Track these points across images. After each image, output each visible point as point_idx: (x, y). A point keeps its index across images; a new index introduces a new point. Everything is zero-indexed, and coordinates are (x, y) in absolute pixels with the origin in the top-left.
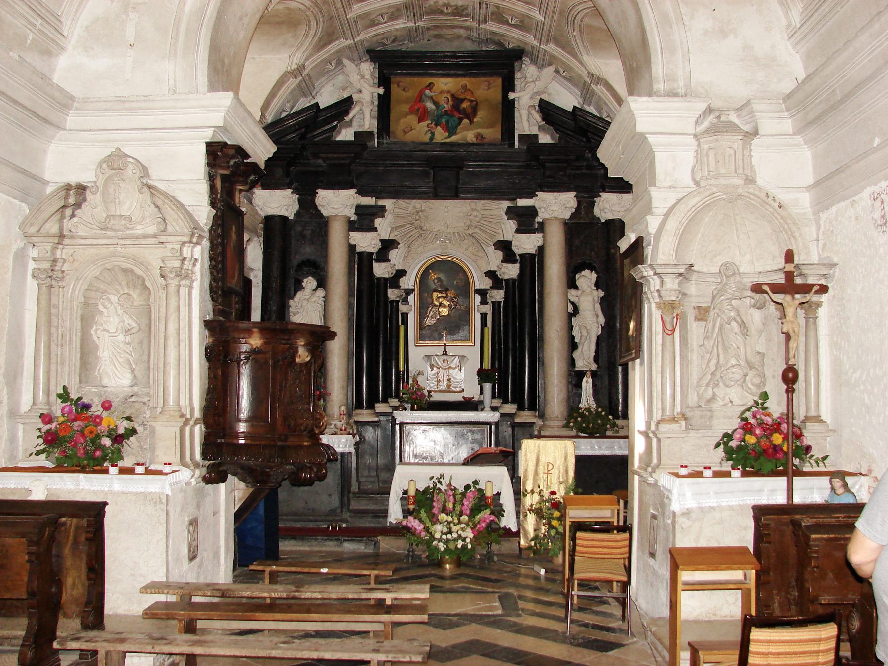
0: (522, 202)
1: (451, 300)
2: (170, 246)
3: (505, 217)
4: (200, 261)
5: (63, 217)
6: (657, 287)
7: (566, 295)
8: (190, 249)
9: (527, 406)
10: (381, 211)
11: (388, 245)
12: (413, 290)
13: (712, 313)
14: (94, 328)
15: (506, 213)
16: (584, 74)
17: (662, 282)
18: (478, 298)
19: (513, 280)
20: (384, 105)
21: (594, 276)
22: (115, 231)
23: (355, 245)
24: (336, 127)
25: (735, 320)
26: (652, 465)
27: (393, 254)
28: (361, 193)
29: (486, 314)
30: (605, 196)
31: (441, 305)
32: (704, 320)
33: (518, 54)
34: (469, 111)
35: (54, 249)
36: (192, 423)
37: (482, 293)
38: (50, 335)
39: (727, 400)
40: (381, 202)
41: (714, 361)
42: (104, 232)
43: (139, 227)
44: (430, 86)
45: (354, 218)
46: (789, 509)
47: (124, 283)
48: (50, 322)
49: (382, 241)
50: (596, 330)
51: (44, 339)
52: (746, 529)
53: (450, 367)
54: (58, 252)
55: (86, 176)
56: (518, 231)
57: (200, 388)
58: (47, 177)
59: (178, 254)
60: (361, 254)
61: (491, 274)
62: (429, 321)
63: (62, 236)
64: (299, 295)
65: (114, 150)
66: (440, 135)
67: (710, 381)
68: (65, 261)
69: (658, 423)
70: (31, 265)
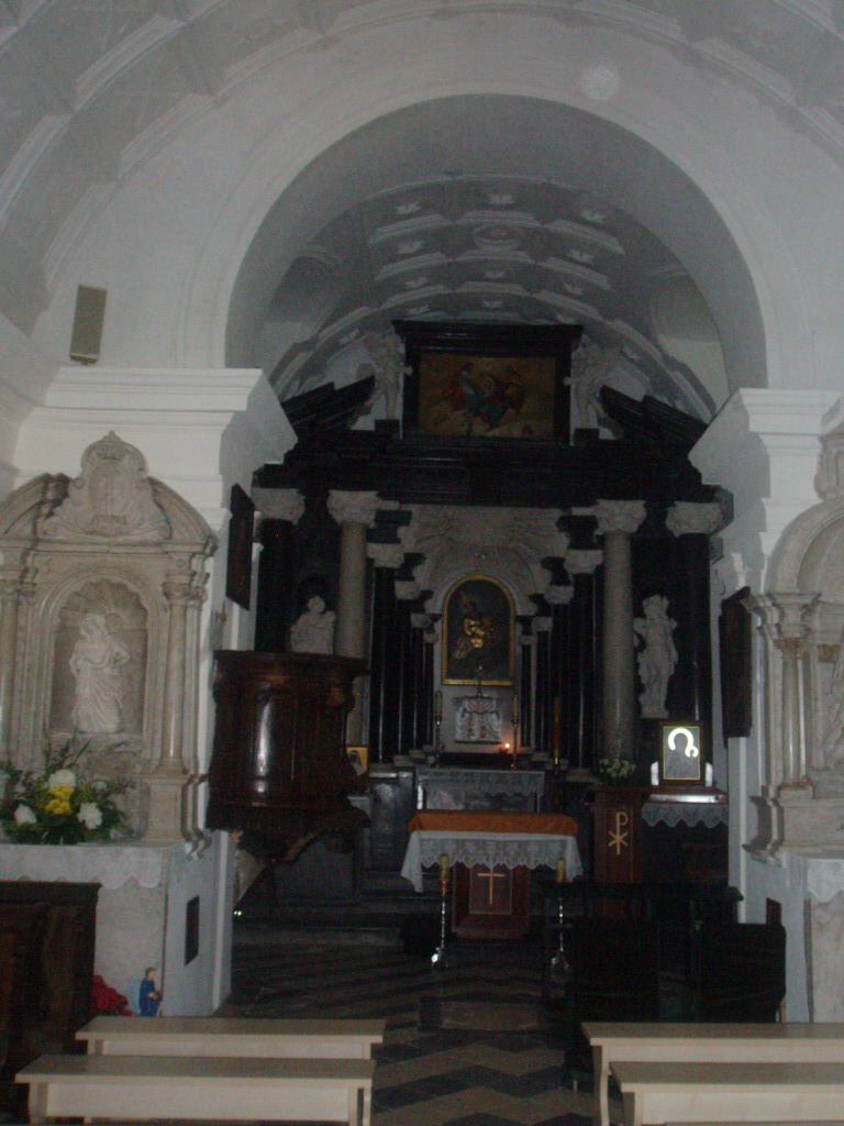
0: (578, 511)
2: (176, 557)
3: (555, 528)
5: (38, 516)
10: (405, 518)
11: (412, 560)
12: (441, 615)
15: (558, 524)
16: (657, 355)
17: (782, 616)
18: (519, 627)
19: (565, 606)
20: (412, 392)
21: (666, 602)
24: (352, 413)
27: (421, 574)
28: (383, 495)
31: (474, 635)
35: (25, 554)
36: (197, 780)
37: (525, 621)
40: (405, 508)
44: (468, 367)
45: (373, 525)
53: (486, 712)
54: (29, 559)
55: (73, 469)
60: (379, 570)
61: (537, 599)
62: (458, 655)
63: (36, 541)
64: (303, 619)
65: (106, 434)
66: (480, 429)
68: (37, 571)
69: (780, 788)
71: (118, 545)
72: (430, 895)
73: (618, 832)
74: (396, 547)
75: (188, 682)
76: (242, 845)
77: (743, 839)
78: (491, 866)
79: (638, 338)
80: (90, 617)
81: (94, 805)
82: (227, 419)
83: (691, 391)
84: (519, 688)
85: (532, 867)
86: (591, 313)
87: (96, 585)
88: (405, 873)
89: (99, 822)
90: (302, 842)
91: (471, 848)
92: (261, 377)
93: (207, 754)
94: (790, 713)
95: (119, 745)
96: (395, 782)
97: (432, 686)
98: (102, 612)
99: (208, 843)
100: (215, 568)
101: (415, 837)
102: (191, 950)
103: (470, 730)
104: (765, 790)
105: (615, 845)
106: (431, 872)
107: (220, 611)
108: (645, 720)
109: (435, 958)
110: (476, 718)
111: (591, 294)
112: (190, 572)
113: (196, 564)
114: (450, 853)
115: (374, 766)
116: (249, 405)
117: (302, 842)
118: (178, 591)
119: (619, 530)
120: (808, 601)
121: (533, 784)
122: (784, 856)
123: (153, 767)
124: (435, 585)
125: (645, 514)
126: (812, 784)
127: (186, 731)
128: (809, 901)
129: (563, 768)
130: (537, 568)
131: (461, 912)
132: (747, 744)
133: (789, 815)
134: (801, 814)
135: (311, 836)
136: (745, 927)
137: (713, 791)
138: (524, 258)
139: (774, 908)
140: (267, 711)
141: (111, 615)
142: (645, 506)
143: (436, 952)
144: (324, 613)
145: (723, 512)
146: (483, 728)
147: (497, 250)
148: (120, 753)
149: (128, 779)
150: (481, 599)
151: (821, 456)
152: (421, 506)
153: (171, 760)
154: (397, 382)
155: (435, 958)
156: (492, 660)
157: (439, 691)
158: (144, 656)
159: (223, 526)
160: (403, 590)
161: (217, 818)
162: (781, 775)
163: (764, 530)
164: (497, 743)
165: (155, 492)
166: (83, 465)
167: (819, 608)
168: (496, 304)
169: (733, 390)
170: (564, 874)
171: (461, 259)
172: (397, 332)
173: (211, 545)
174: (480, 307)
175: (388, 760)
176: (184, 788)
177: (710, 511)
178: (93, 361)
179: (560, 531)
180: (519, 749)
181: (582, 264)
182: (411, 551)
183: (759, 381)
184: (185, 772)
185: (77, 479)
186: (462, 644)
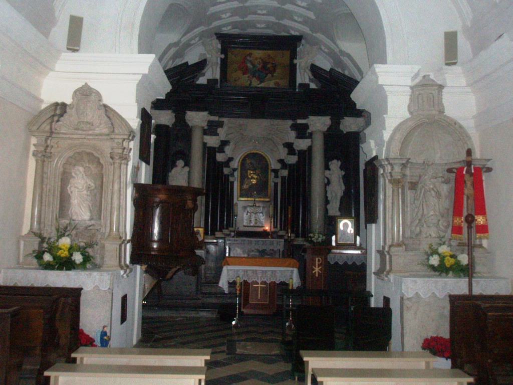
0: (299, 121)
1: (258, 175)
2: (116, 141)
3: (290, 129)
5: (51, 123)
6: (390, 171)
8: (127, 143)
10: (221, 124)
11: (224, 143)
13: (420, 186)
14: (69, 186)
15: (290, 127)
16: (337, 50)
17: (392, 169)
19: (294, 165)
20: (224, 64)
21: (339, 163)
22: (83, 130)
23: (206, 143)
24: (197, 76)
25: (433, 189)
26: (386, 270)
27: (228, 149)
28: (211, 114)
29: (277, 183)
30: (346, 118)
31: (252, 178)
32: (415, 190)
33: (298, 39)
34: (271, 69)
35: (46, 140)
36: (126, 242)
37: (276, 171)
38: (42, 189)
39: (428, 235)
41: (421, 213)
43: (97, 129)
44: (250, 55)
48: (42, 182)
49: (222, 141)
50: (340, 194)
51: (38, 191)
52: (444, 308)
54: (49, 142)
55: (68, 100)
57: (130, 225)
58: (42, 97)
59: (121, 145)
60: (210, 148)
61: (281, 161)
62: (245, 187)
63: (52, 133)
65: (84, 84)
66: (255, 83)
67: (418, 224)
68: (52, 147)
69: (390, 246)
70: (32, 148)
72: (232, 294)
73: (317, 267)
74: (217, 137)
75: (122, 197)
76: (146, 271)
78: (259, 281)
80: (77, 168)
81: (79, 253)
82: (139, 77)
86: (305, 29)
87: (79, 153)
88: (220, 284)
89: (81, 260)
90: (174, 270)
95: (90, 226)
96: (216, 244)
100: (134, 146)
101: (225, 269)
102: (124, 318)
103: (250, 221)
104: (384, 247)
105: (315, 273)
106: (232, 284)
107: (136, 166)
109: (234, 323)
110: (253, 215)
111: (306, 21)
117: (174, 270)
120: (404, 162)
121: (279, 245)
122: (391, 277)
124: (235, 154)
129: (292, 238)
130: (281, 147)
132: (376, 227)
134: (400, 258)
135: (178, 267)
139: (387, 300)
140: (158, 211)
143: (234, 320)
145: (366, 122)
146: (256, 220)
148: (90, 229)
149: (95, 241)
150: (256, 161)
151: (411, 96)
155: (234, 323)
156: (261, 189)
157: (236, 203)
159: (138, 126)
160: (220, 157)
161: (135, 259)
163: (385, 130)
164: (263, 227)
165: (106, 111)
166: (73, 98)
168: (263, 26)
169: (371, 65)
176: (120, 246)
177: (360, 121)
178: (77, 50)
179: (292, 130)
180: (273, 230)
183: (384, 61)
184: (121, 238)
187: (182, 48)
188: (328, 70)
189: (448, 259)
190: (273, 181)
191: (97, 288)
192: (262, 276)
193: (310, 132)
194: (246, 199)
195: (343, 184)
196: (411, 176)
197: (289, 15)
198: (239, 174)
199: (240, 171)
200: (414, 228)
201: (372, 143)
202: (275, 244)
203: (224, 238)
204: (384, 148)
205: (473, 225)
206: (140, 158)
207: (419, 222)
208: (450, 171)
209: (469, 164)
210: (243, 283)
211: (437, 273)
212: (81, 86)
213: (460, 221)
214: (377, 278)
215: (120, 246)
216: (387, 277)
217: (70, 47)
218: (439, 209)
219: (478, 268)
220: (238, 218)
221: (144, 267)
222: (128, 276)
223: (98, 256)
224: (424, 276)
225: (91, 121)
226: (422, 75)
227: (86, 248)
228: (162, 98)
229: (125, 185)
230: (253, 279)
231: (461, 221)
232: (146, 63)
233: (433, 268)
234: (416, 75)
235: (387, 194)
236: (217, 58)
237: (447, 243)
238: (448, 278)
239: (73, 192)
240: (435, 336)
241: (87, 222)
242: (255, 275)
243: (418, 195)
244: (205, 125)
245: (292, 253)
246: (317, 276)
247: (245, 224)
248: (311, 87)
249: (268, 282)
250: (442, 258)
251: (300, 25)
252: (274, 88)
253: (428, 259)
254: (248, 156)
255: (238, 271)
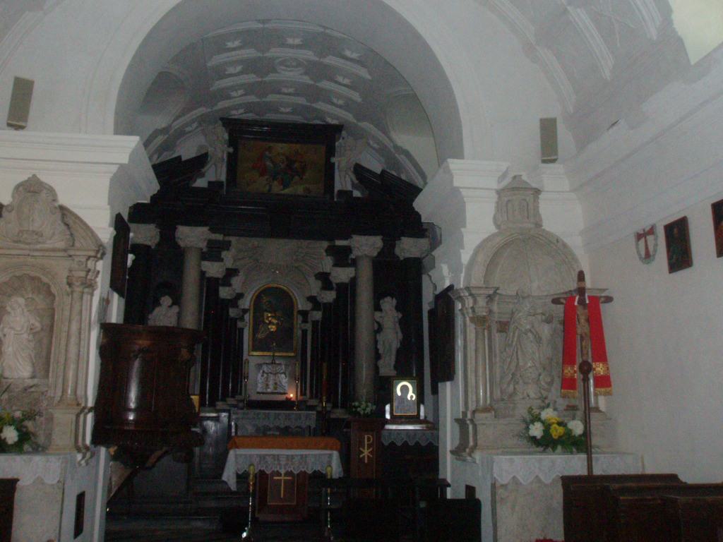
0: (339, 243)
3: (325, 254)
4: (101, 274)
6: (471, 305)
7: (373, 315)
8: (94, 262)
9: (339, 405)
10: (226, 246)
11: (231, 273)
13: (512, 327)
15: (326, 251)
16: (390, 145)
17: (475, 302)
18: (300, 318)
19: (330, 304)
20: (232, 162)
21: (394, 301)
23: (205, 272)
25: (530, 331)
27: (236, 282)
28: (213, 230)
29: (307, 330)
30: (404, 239)
31: (270, 323)
33: (338, 129)
36: (86, 411)
37: (304, 314)
39: (525, 394)
40: (227, 238)
41: (514, 364)
42: (16, 244)
43: (48, 242)
44: (270, 149)
46: (590, 479)
47: (29, 289)
49: (227, 269)
50: (396, 345)
56: (336, 265)
57: (95, 381)
60: (210, 279)
61: (312, 299)
62: (259, 336)
65: (31, 176)
66: (277, 188)
69: (474, 412)
71: (37, 250)
72: (242, 494)
73: (366, 447)
74: (222, 264)
75: (82, 342)
76: (115, 458)
77: (449, 447)
78: (283, 472)
79: (379, 134)
80: (14, 299)
81: (12, 428)
82: (114, 169)
83: (409, 166)
84: (299, 358)
85: (310, 472)
86: (349, 117)
87: (18, 278)
88: (224, 478)
89: (16, 439)
90: (158, 453)
91: (269, 460)
92: (139, 142)
93: (94, 393)
94: (480, 363)
95: (31, 387)
96: (217, 419)
97: (242, 356)
98: (23, 296)
99: (93, 455)
100: (103, 267)
101: (232, 453)
102: (78, 529)
103: (267, 385)
104: (465, 414)
105: (364, 456)
106: (242, 478)
107: (106, 297)
108: (381, 377)
109: (245, 535)
110: (272, 377)
111: (348, 106)
112: (87, 269)
113: (90, 264)
114: (255, 464)
115: (202, 408)
116: (130, 159)
117: (158, 453)
118: (77, 282)
119: (365, 255)
120: (491, 292)
121: (308, 419)
122: (478, 456)
123: (56, 402)
124: (246, 289)
125: (382, 244)
126: (494, 410)
127: (80, 375)
128: (495, 484)
129: (328, 409)
130: (312, 280)
131: (262, 502)
132: (452, 386)
133: (480, 428)
134: (488, 428)
135: (165, 449)
136: (452, 501)
137: (425, 421)
138: (307, 80)
139: (470, 490)
140: (137, 364)
141: (28, 298)
142: (382, 239)
143: (245, 531)
144: (170, 307)
145: (431, 244)
146: (276, 384)
147: (291, 74)
148: (33, 392)
149: (37, 410)
150: (276, 299)
151: (497, 203)
152: (237, 238)
153: (68, 396)
154: (223, 157)
155: (245, 535)
156: (281, 340)
157: (247, 360)
158: (52, 327)
159: (110, 239)
160: (224, 293)
161: (99, 438)
162: (475, 404)
163: (463, 248)
164: (285, 393)
165: (63, 215)
166: (13, 197)
167: (497, 298)
168: (288, 110)
169: (441, 161)
170: (331, 474)
171: (267, 79)
172: (224, 126)
173: (101, 251)
174: (277, 111)
175: (212, 405)
176: (78, 416)
177: (424, 242)
178: (22, 128)
179: (327, 255)
180: (300, 398)
181: (345, 85)
182: (230, 267)
183: (459, 155)
184: (78, 404)
185: (8, 206)
186: (263, 329)
187: (173, 136)
188: (379, 173)
189: (555, 428)
190: (301, 328)
191: (39, 481)
192: (287, 464)
193: (354, 257)
194: (261, 353)
195: (399, 330)
196: (499, 313)
197: (326, 97)
198: (251, 317)
199: (254, 313)
200: (505, 386)
201: (445, 269)
202: (303, 418)
203: (228, 411)
204: (463, 275)
205: (591, 376)
206: (111, 287)
207: (512, 378)
208: (556, 301)
209: (581, 291)
210: (258, 476)
211: (541, 449)
212: (26, 179)
213: (572, 372)
214: (456, 459)
215: (78, 416)
216: (470, 456)
217: (14, 123)
218: (540, 357)
219: (595, 441)
220: (250, 382)
221: (112, 450)
222: (87, 464)
223: (41, 432)
224: (523, 453)
225: (40, 229)
226: (511, 175)
227: (23, 420)
228: (146, 202)
229: (87, 325)
230: (273, 469)
231: (573, 371)
232: (125, 148)
233: (534, 440)
234: (504, 176)
235: (468, 337)
236: (223, 152)
237: (551, 405)
238: (556, 455)
239: (7, 336)
240: (542, 538)
241: (26, 380)
242: (276, 462)
243: (511, 339)
244: (203, 245)
245: (327, 429)
246: (366, 461)
247: (259, 390)
248: (354, 196)
249: (296, 473)
250: (547, 427)
251: (338, 110)
252: (303, 197)
253: (527, 428)
254: (266, 291)
255: (251, 456)
